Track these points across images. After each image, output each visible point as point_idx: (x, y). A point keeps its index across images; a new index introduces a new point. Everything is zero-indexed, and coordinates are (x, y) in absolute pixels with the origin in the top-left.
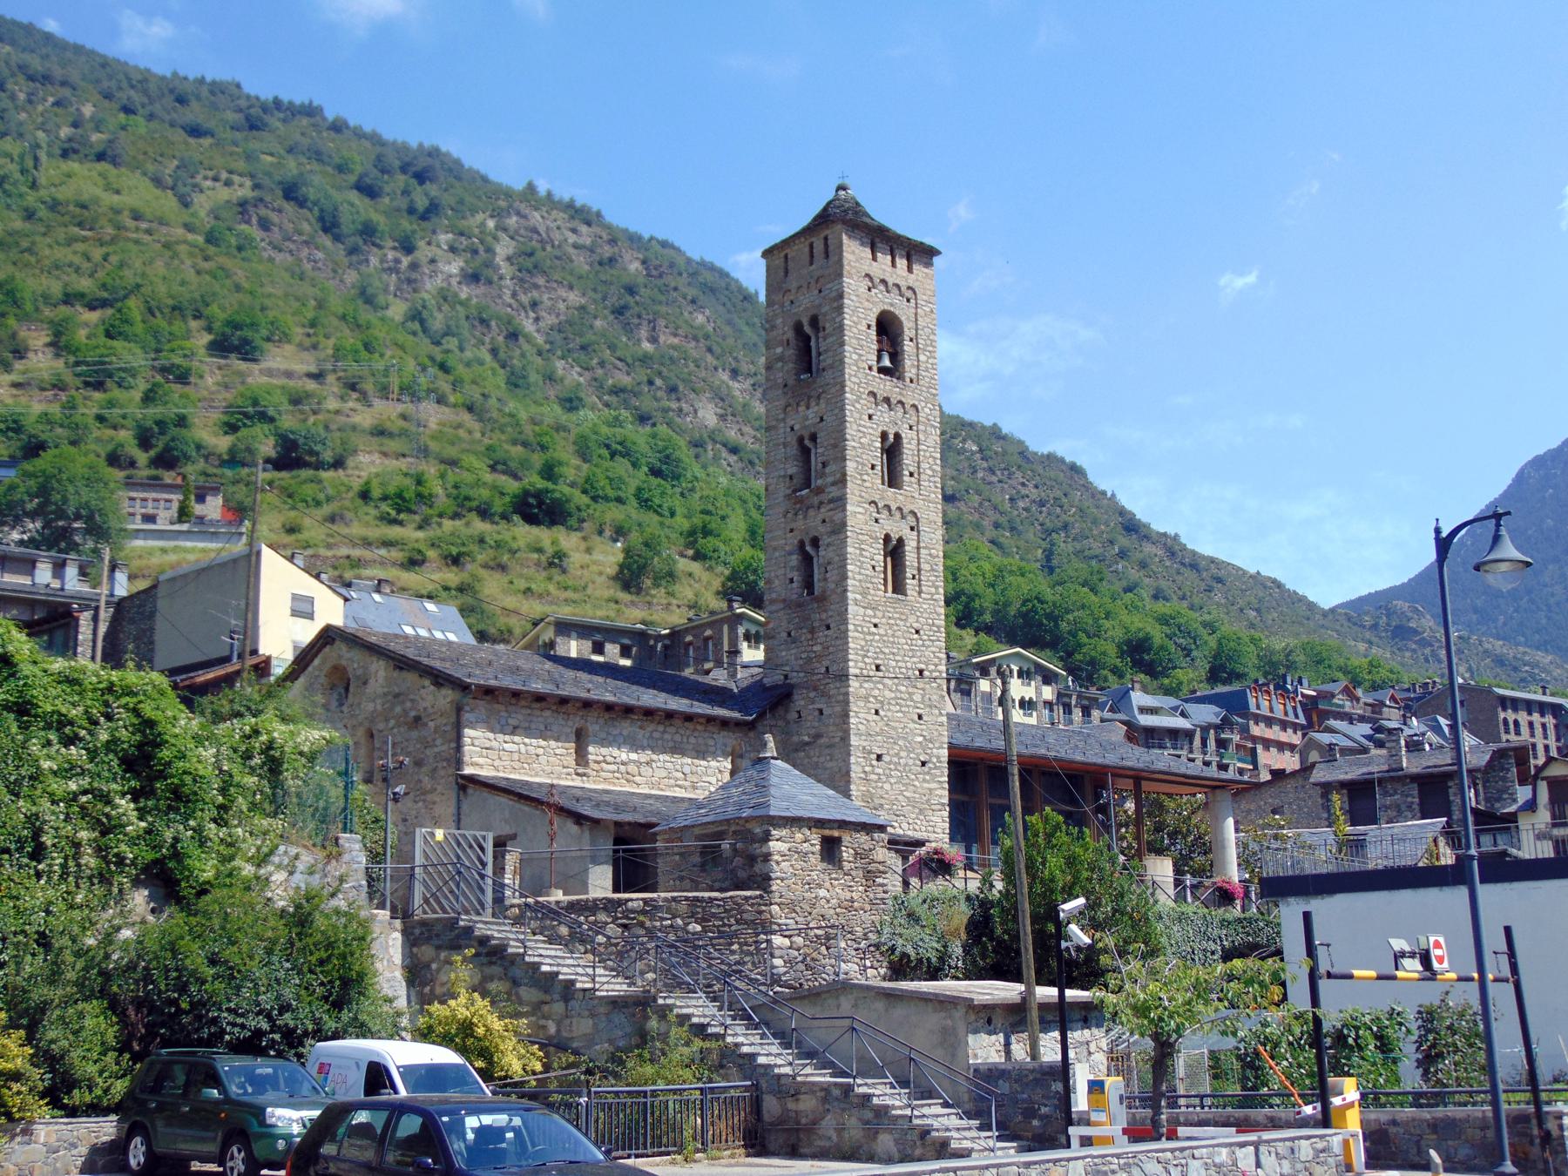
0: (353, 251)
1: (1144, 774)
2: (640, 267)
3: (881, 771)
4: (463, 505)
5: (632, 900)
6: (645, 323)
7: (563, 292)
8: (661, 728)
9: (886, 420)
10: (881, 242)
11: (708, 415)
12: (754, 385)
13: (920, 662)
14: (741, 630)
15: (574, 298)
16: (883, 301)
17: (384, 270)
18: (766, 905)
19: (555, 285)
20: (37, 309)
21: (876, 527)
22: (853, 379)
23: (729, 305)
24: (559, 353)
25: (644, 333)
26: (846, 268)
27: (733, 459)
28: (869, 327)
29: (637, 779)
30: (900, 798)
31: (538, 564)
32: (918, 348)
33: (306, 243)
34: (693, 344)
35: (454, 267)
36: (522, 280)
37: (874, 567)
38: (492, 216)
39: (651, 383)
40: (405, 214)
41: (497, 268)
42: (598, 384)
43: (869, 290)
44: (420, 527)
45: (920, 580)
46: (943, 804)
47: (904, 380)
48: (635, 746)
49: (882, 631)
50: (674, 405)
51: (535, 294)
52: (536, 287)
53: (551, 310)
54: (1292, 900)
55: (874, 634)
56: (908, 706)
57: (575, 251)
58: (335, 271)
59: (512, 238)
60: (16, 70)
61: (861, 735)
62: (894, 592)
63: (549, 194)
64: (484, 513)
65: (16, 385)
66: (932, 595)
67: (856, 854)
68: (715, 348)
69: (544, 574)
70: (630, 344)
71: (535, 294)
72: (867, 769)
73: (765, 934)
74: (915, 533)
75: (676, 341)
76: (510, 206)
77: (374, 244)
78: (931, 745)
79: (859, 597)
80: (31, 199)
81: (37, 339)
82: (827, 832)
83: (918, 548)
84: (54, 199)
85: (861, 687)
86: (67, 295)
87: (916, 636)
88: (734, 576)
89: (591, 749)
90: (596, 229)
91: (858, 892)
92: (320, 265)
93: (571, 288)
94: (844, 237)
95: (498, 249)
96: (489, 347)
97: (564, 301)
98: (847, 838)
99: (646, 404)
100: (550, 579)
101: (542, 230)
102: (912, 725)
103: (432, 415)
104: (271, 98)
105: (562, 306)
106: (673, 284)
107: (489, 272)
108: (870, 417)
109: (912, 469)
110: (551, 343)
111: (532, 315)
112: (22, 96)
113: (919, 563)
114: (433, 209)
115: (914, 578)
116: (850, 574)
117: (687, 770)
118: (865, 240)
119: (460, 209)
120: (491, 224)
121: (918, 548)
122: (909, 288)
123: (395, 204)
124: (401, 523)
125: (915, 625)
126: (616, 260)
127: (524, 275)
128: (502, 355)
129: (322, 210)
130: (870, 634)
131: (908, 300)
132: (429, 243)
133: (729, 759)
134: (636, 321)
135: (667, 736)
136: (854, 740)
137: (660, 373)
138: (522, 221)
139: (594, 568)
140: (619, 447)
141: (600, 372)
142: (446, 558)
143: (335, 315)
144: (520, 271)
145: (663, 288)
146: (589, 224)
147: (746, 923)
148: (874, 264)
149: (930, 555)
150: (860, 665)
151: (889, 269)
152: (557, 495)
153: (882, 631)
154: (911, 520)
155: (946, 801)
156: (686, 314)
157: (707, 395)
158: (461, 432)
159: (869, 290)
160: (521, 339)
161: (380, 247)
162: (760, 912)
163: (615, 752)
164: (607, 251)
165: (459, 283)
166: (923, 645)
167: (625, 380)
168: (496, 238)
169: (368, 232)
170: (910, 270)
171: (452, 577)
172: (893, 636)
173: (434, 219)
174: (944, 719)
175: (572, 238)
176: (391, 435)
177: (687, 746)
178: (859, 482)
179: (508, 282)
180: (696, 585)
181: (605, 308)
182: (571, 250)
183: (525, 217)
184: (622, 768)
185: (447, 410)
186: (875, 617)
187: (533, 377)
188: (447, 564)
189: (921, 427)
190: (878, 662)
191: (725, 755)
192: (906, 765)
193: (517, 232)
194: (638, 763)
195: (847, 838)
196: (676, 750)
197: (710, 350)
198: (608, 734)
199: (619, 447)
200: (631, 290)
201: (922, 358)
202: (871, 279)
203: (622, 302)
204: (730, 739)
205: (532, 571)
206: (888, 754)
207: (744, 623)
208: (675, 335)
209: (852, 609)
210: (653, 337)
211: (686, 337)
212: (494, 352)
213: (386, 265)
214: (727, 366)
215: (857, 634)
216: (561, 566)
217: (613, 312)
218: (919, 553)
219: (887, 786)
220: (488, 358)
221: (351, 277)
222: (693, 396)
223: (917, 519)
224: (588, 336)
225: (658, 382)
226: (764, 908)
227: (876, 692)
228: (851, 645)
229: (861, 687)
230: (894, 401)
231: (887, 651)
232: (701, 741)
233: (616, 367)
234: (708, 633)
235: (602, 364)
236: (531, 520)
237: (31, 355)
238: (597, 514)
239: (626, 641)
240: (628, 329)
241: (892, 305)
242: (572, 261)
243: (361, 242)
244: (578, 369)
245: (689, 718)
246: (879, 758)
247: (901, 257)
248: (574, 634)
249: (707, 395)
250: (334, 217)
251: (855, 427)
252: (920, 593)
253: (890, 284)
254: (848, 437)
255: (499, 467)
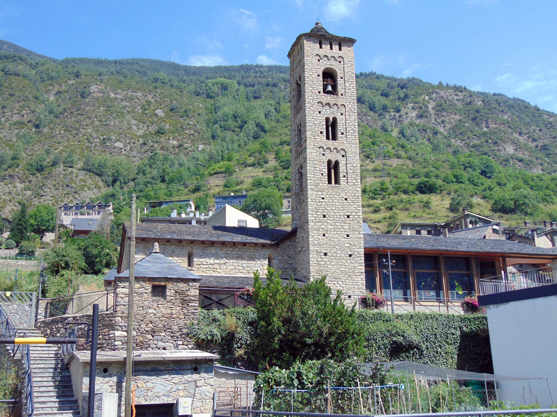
0: (380, 115)
1: (506, 255)
2: (482, 103)
3: (326, 260)
4: (398, 190)
5: (69, 317)
6: (484, 122)
7: (453, 116)
8: (231, 249)
9: (329, 113)
10: (325, 40)
11: (510, 150)
12: (528, 137)
13: (348, 212)
14: (468, 220)
15: (457, 117)
16: (325, 64)
17: (390, 119)
18: (113, 317)
19: (450, 114)
20: (272, 148)
21: (323, 157)
22: (310, 98)
23: (519, 111)
24: (453, 137)
25: (484, 125)
26: (306, 53)
27: (520, 164)
28: (319, 76)
29: (219, 270)
30: (338, 271)
31: (420, 207)
32: (345, 81)
33: (365, 115)
34: (503, 126)
35: (414, 114)
36: (438, 115)
37: (322, 174)
38: (427, 95)
39: (487, 142)
40: (397, 100)
41: (429, 112)
42: (468, 145)
43: (319, 60)
44: (382, 199)
45: (347, 177)
46: (362, 273)
47: (337, 95)
48: (217, 257)
49: (326, 201)
50: (496, 148)
51: (443, 118)
52: (443, 116)
53: (449, 123)
54: (491, 306)
55: (323, 202)
56: (341, 231)
57: (457, 102)
58: (374, 122)
59: (434, 101)
60: (281, 79)
61: (315, 245)
62: (335, 184)
63: (447, 84)
64: (405, 192)
65: (264, 172)
66: (354, 183)
67: (176, 292)
68: (511, 126)
69: (422, 210)
70: (479, 130)
71: (443, 118)
72: (319, 259)
73: (112, 330)
74: (345, 158)
75: (496, 126)
76: (433, 91)
77: (387, 112)
78: (354, 247)
79: (313, 187)
80: (278, 117)
81: (271, 157)
82: (156, 283)
83: (346, 164)
84: (285, 115)
85: (315, 225)
86: (281, 142)
87: (346, 201)
88: (495, 203)
89: (195, 260)
90: (464, 93)
91: (176, 310)
92: (369, 121)
93: (456, 114)
94: (305, 41)
95: (429, 106)
96: (427, 138)
97: (454, 119)
98: (169, 286)
99: (485, 149)
100: (424, 211)
101: (445, 97)
102: (343, 239)
103: (395, 162)
104: (359, 73)
105: (453, 120)
106: (494, 107)
107: (426, 114)
108: (320, 112)
109: (342, 131)
110: (450, 134)
111: (442, 125)
112: (283, 87)
113: (347, 170)
114: (406, 96)
115: (344, 176)
116: (308, 178)
117: (244, 265)
118: (316, 41)
119: (416, 95)
120: (427, 98)
121: (346, 164)
122: (339, 57)
123: (394, 97)
124: (376, 199)
125: (344, 197)
126: (472, 102)
127: (439, 113)
128: (432, 140)
129: (369, 104)
130: (319, 202)
131: (340, 62)
132: (405, 108)
133: (267, 260)
134: (480, 121)
135: (234, 252)
136: (311, 248)
137: (490, 138)
138: (438, 95)
139: (441, 206)
140: (468, 165)
141: (468, 141)
142: (387, 208)
143: (367, 135)
144: (437, 111)
145: (491, 109)
146: (462, 92)
147: (106, 326)
148: (321, 50)
149: (353, 166)
150: (314, 215)
151: (329, 51)
152: (431, 182)
153: (326, 201)
154: (343, 153)
155: (363, 271)
156: (500, 116)
157: (509, 143)
158: (405, 167)
159: (319, 60)
160: (438, 134)
161: (389, 112)
162: (111, 321)
163: (208, 260)
164: (469, 99)
165: (416, 119)
166: (349, 205)
167: (477, 142)
168: (428, 102)
169: (385, 108)
170: (340, 49)
171: (388, 214)
172: (332, 202)
173: (407, 100)
174: (362, 236)
175: (456, 98)
176: (379, 171)
177: (244, 256)
178: (314, 139)
179: (433, 116)
180: (481, 208)
181: (469, 119)
182: (456, 102)
183: (438, 93)
184: (211, 266)
185: (401, 160)
186: (322, 195)
187: (442, 146)
188: (388, 210)
189: (347, 113)
190: (324, 214)
191: (264, 258)
192: (340, 257)
193: (436, 99)
194: (219, 264)
195: (169, 286)
196: (239, 257)
197: (509, 127)
198: (204, 253)
199: (468, 165)
200: (478, 111)
201: (347, 84)
202: (319, 56)
203: (475, 116)
204: (268, 252)
205: (417, 210)
206: (330, 252)
207: (469, 217)
208: (496, 124)
209: (309, 192)
210: (487, 126)
211: (500, 124)
212: (429, 140)
213: (391, 118)
214: (517, 132)
215: (312, 203)
216: (428, 207)
217: (472, 120)
218: (346, 166)
219: (330, 266)
220: (427, 142)
221: (380, 123)
222: (504, 144)
223: (346, 152)
224: (462, 130)
225: (490, 141)
226: (112, 319)
227: (324, 227)
228: (309, 208)
229: (315, 225)
230: (331, 104)
231: (329, 209)
232: (252, 253)
233: (473, 138)
234: (458, 223)
235: (468, 138)
236: (422, 192)
237: (269, 162)
238: (448, 188)
239: (429, 229)
240: (478, 124)
241: (331, 65)
242: (456, 105)
243: (382, 112)
244: (460, 141)
245: (244, 244)
246: (325, 254)
247: (335, 45)
248: (408, 228)
249: (509, 143)
250: (374, 105)
251: (311, 117)
252: (347, 183)
253: (329, 57)
254: (307, 121)
255: (416, 176)
